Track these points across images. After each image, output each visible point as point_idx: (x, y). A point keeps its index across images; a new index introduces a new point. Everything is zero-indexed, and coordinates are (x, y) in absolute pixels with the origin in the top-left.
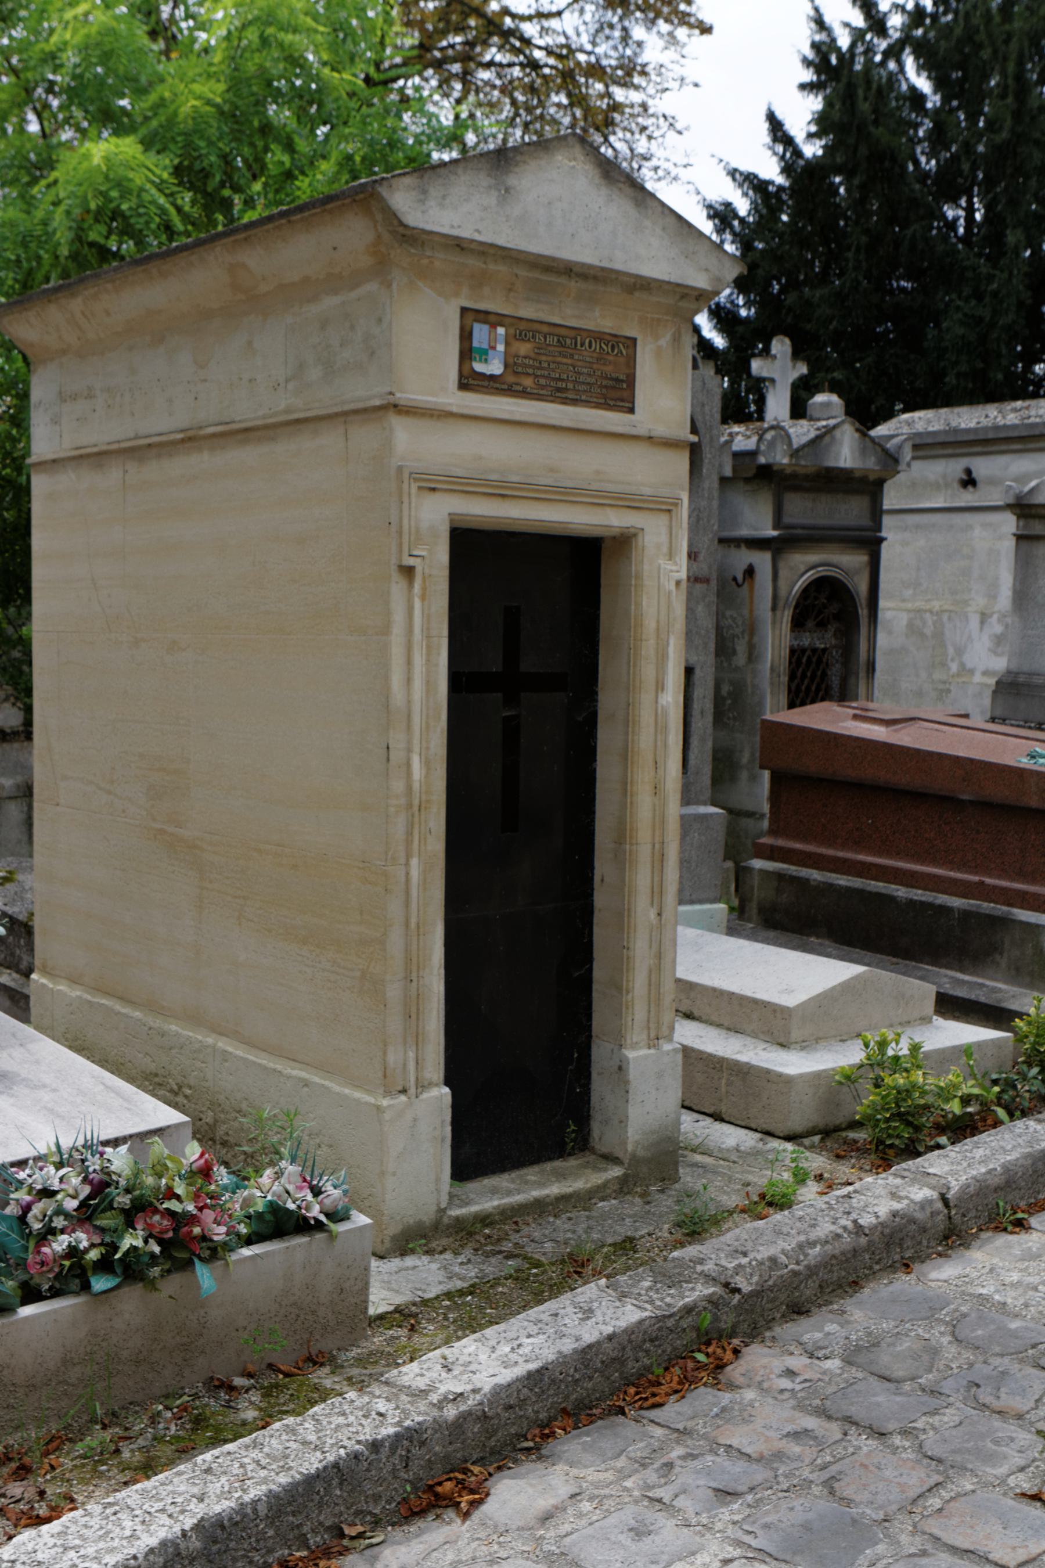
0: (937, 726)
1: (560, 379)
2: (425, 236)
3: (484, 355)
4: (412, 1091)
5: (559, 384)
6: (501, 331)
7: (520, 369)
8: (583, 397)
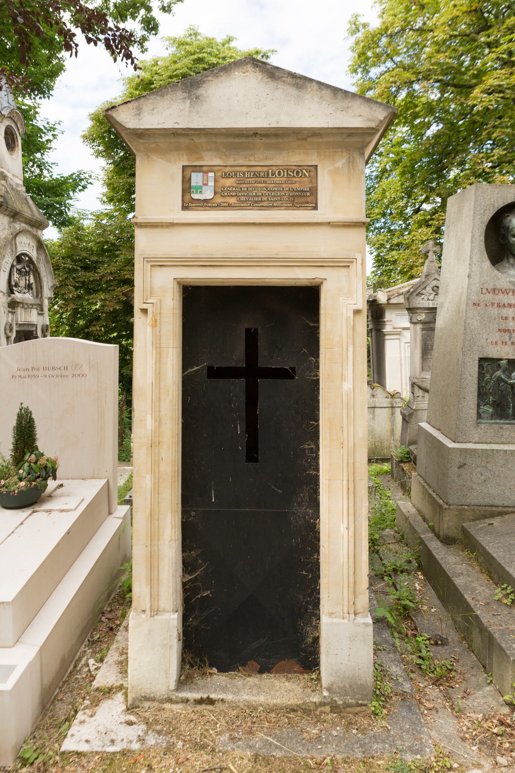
1: (256, 196)
2: (148, 132)
3: (199, 190)
5: (256, 199)
6: (211, 174)
7: (226, 194)
8: (275, 205)
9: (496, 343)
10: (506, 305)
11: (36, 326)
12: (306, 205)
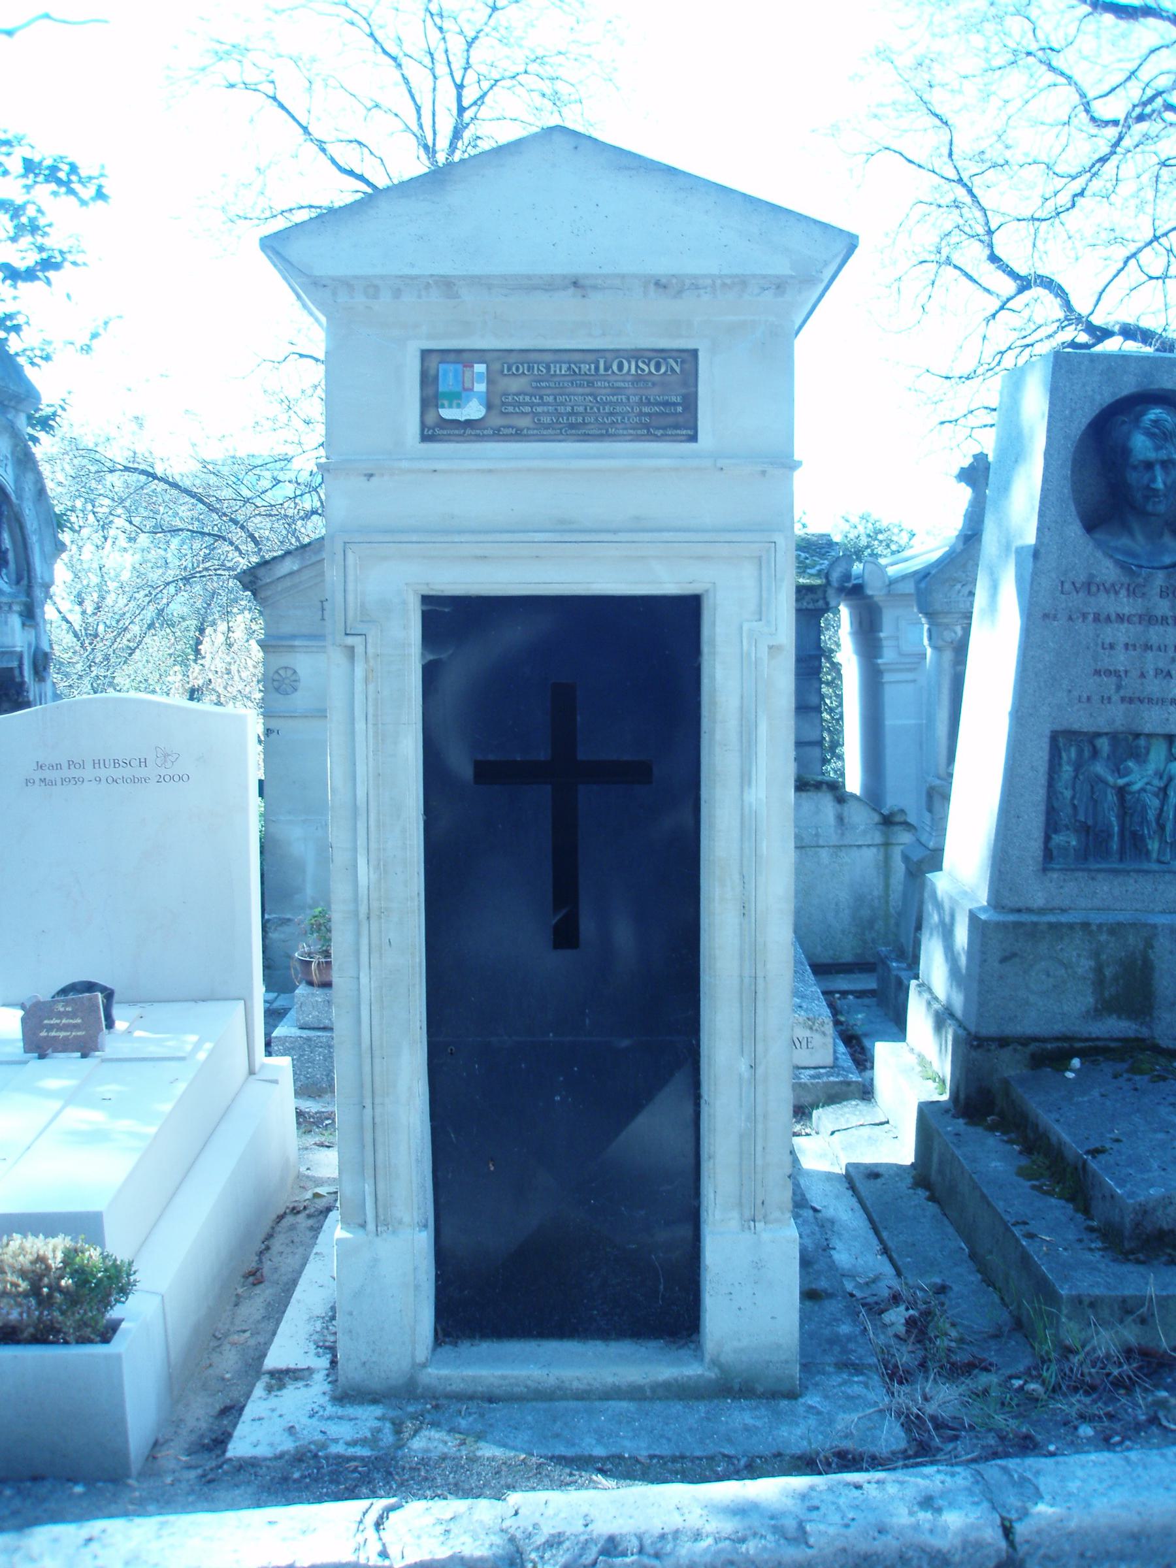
0: (567, 537)
1: (573, 413)
4: (371, 1226)
5: (573, 419)
7: (511, 409)
9: (1089, 699)
10: (1113, 617)
11: (20, 657)
12: (675, 432)
